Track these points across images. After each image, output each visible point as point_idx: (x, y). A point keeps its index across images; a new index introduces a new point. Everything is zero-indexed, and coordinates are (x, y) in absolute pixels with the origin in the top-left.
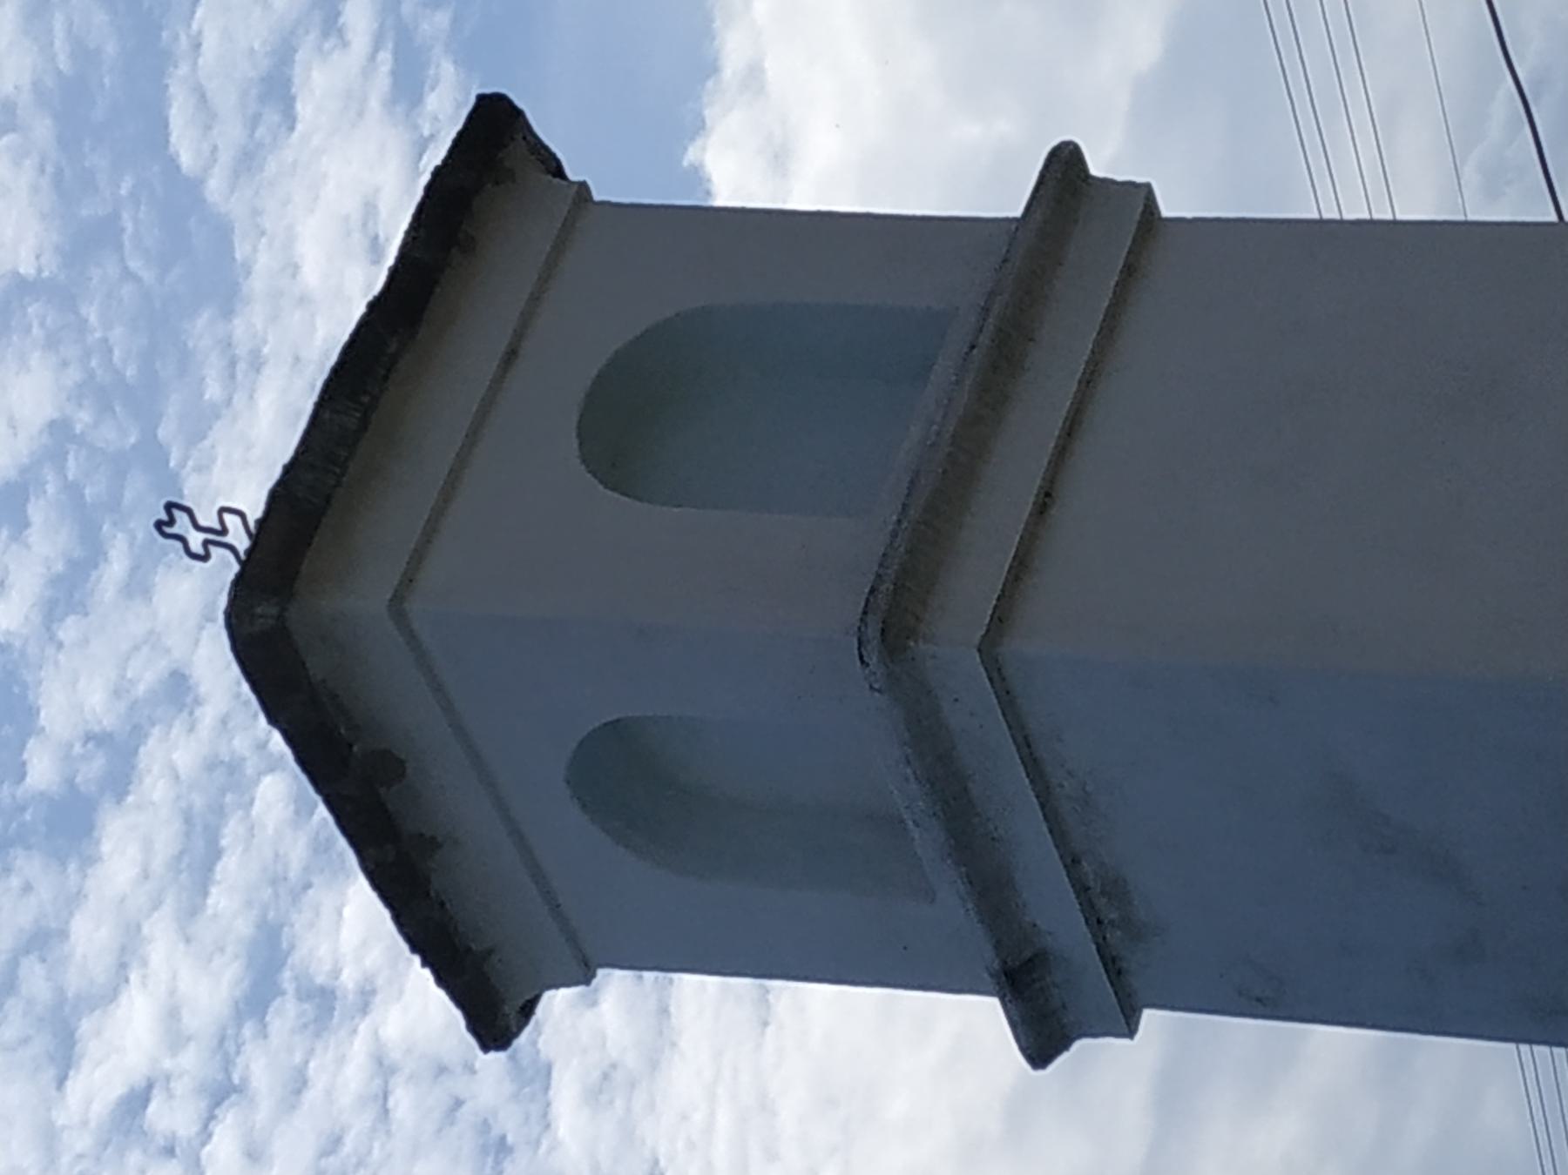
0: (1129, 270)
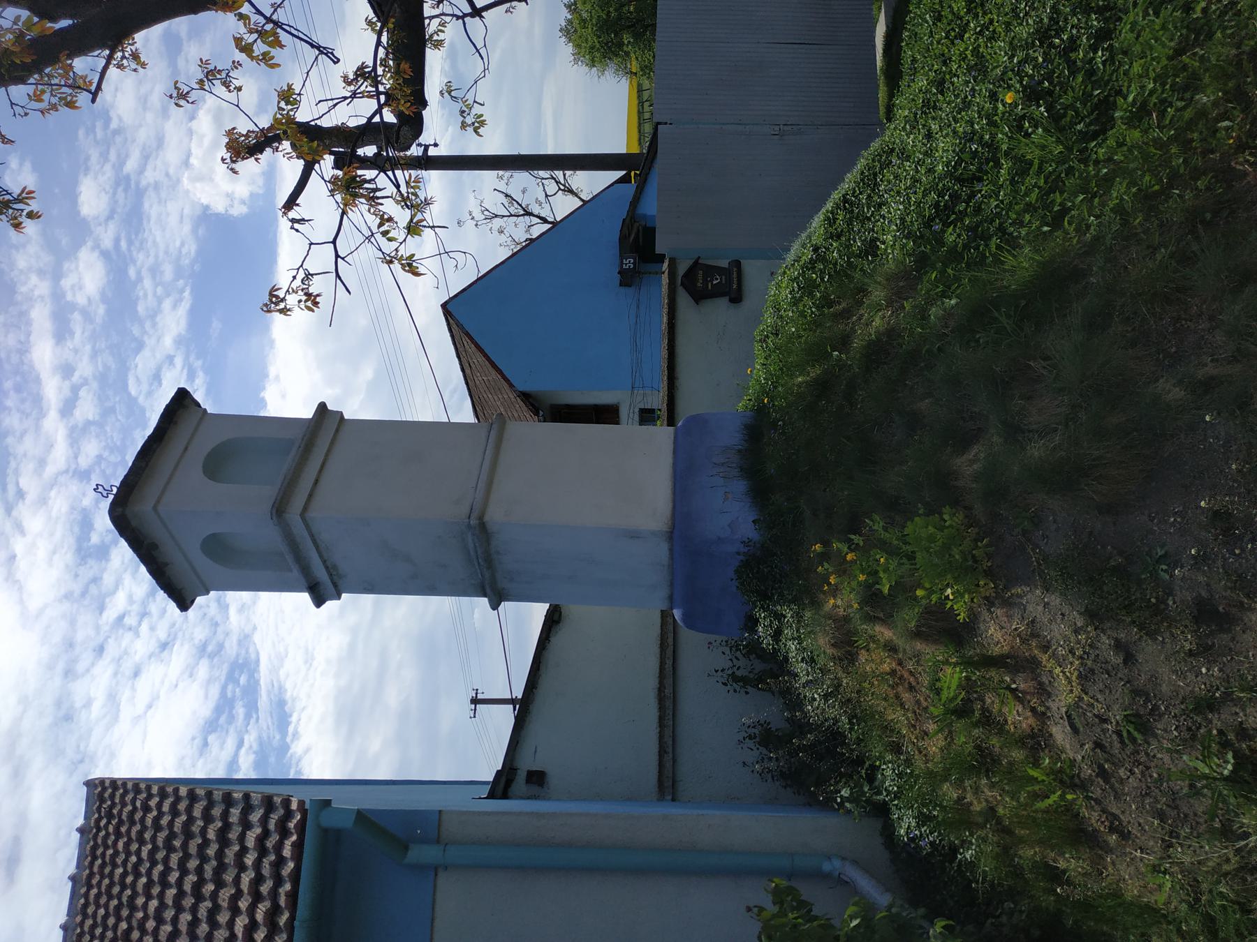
0: (337, 430)
